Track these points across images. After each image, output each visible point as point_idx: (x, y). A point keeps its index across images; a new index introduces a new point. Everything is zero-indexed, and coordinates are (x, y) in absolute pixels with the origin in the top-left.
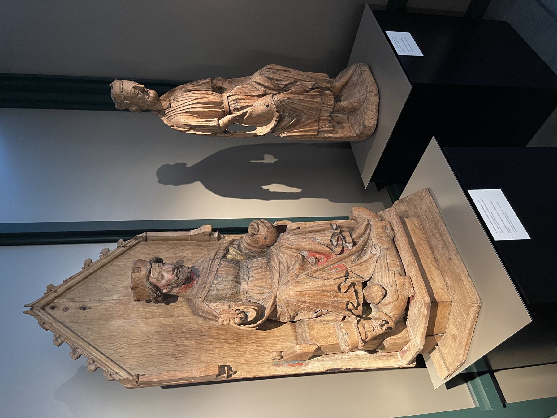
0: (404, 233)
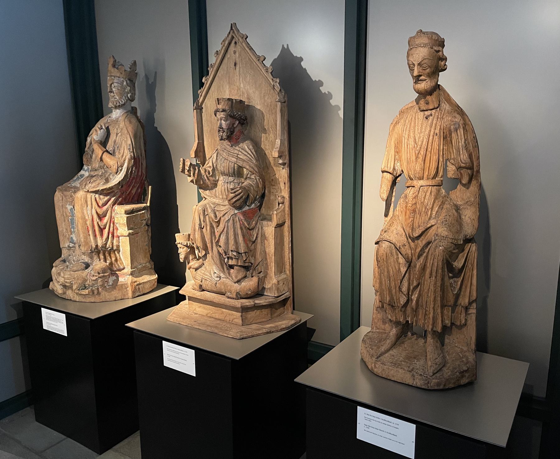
0: (220, 303)
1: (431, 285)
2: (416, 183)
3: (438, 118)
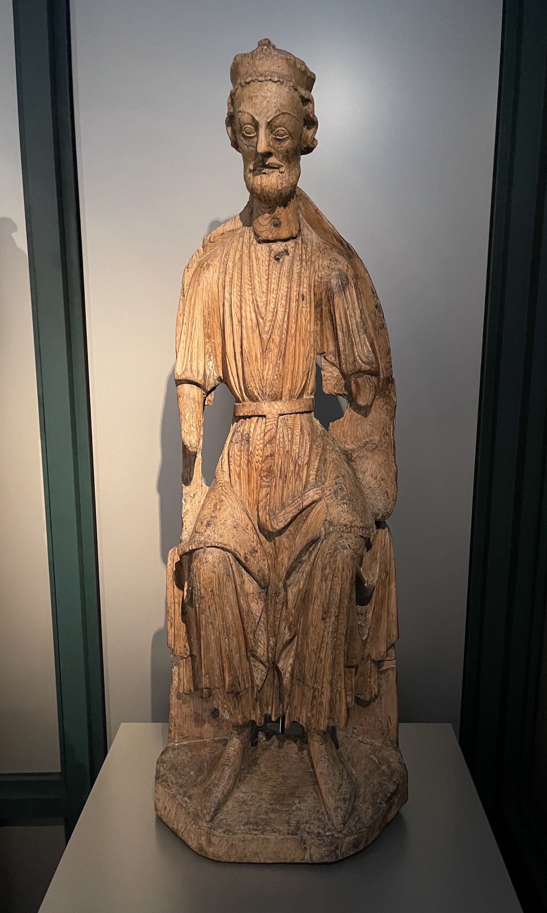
1: (326, 634)
2: (268, 409)
3: (301, 260)
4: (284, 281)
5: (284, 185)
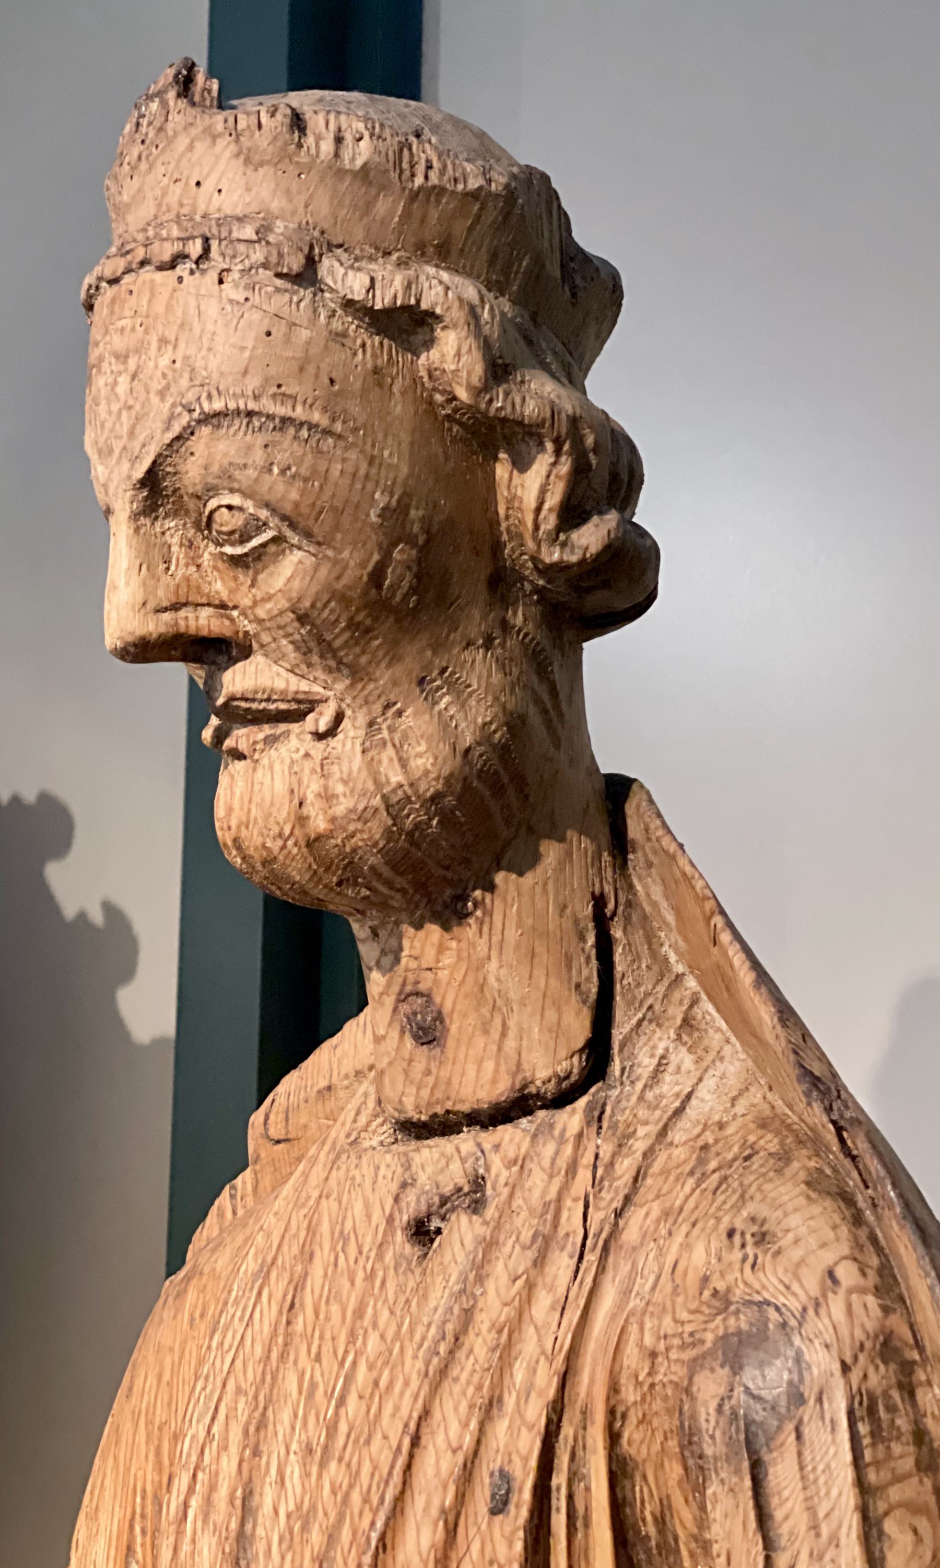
4: (407, 1383)
5: (340, 809)
